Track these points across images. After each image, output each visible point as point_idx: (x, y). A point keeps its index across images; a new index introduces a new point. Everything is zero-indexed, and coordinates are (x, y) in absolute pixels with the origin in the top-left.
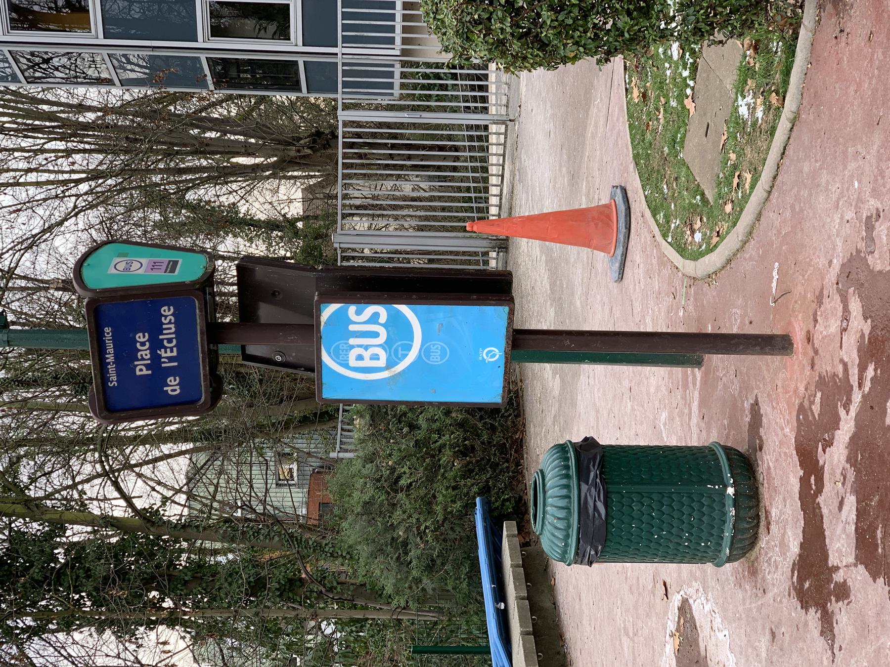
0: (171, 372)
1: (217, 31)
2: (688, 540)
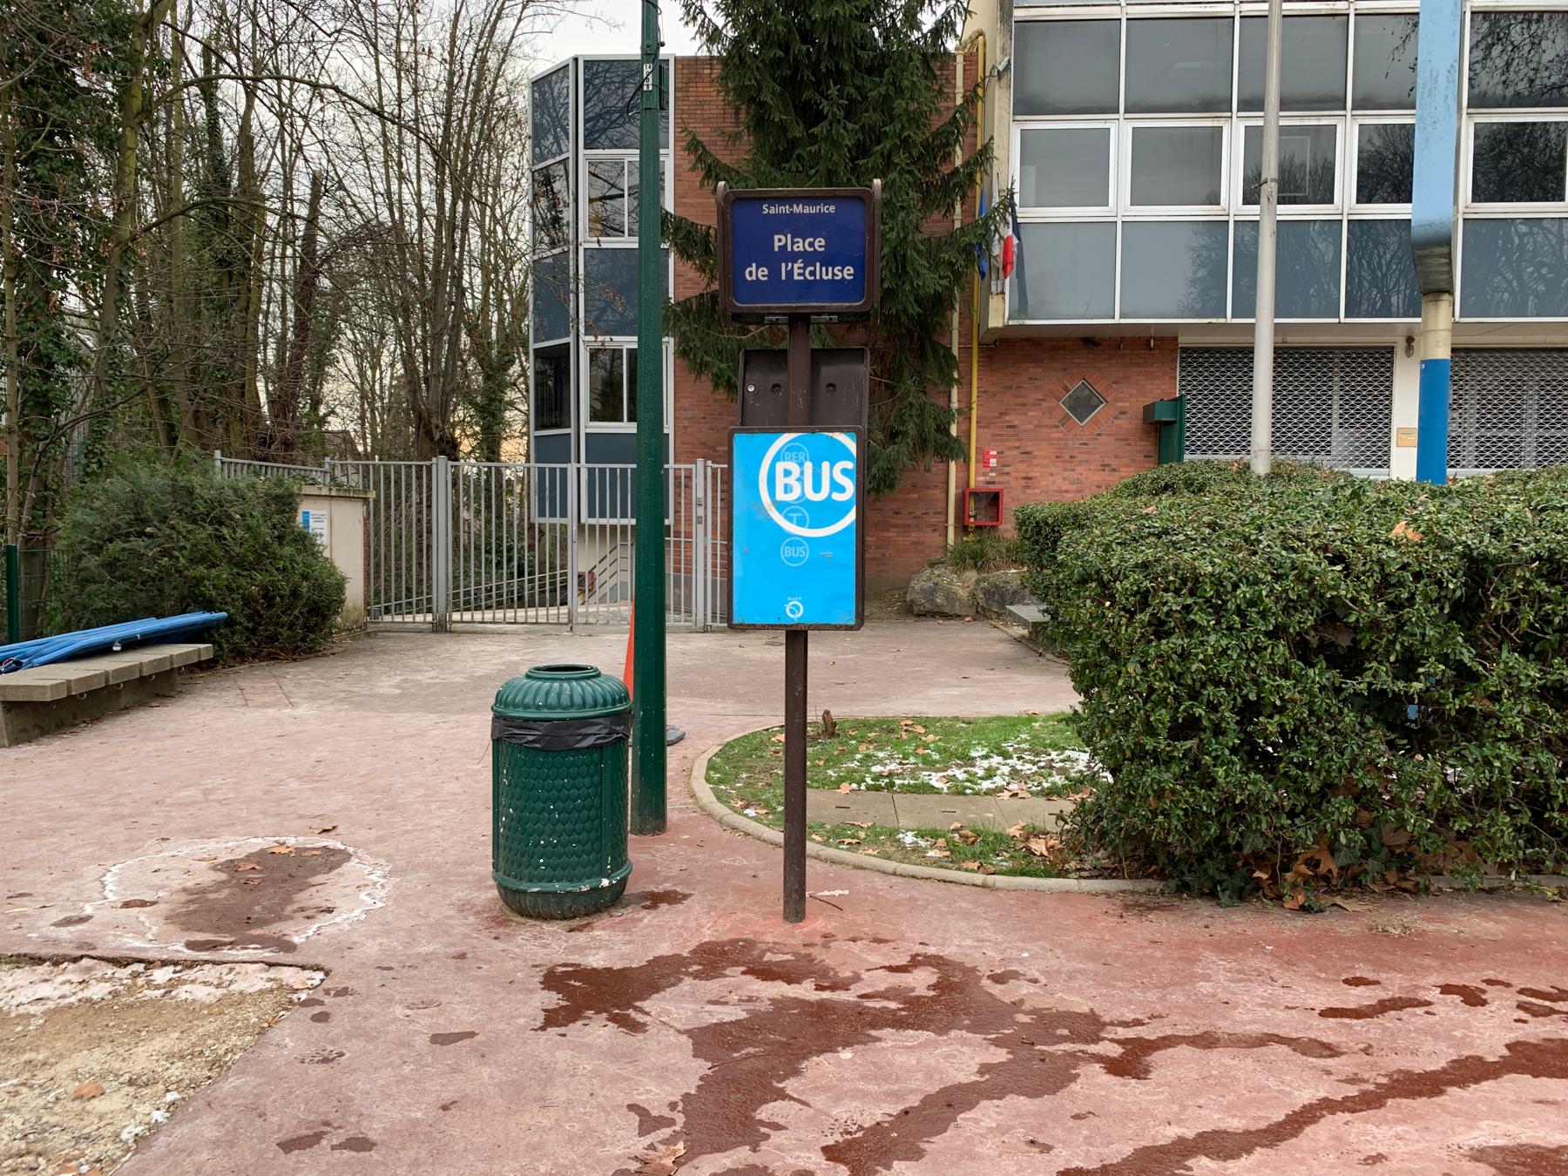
0: (774, 273)
1: (594, 354)
2: (548, 843)
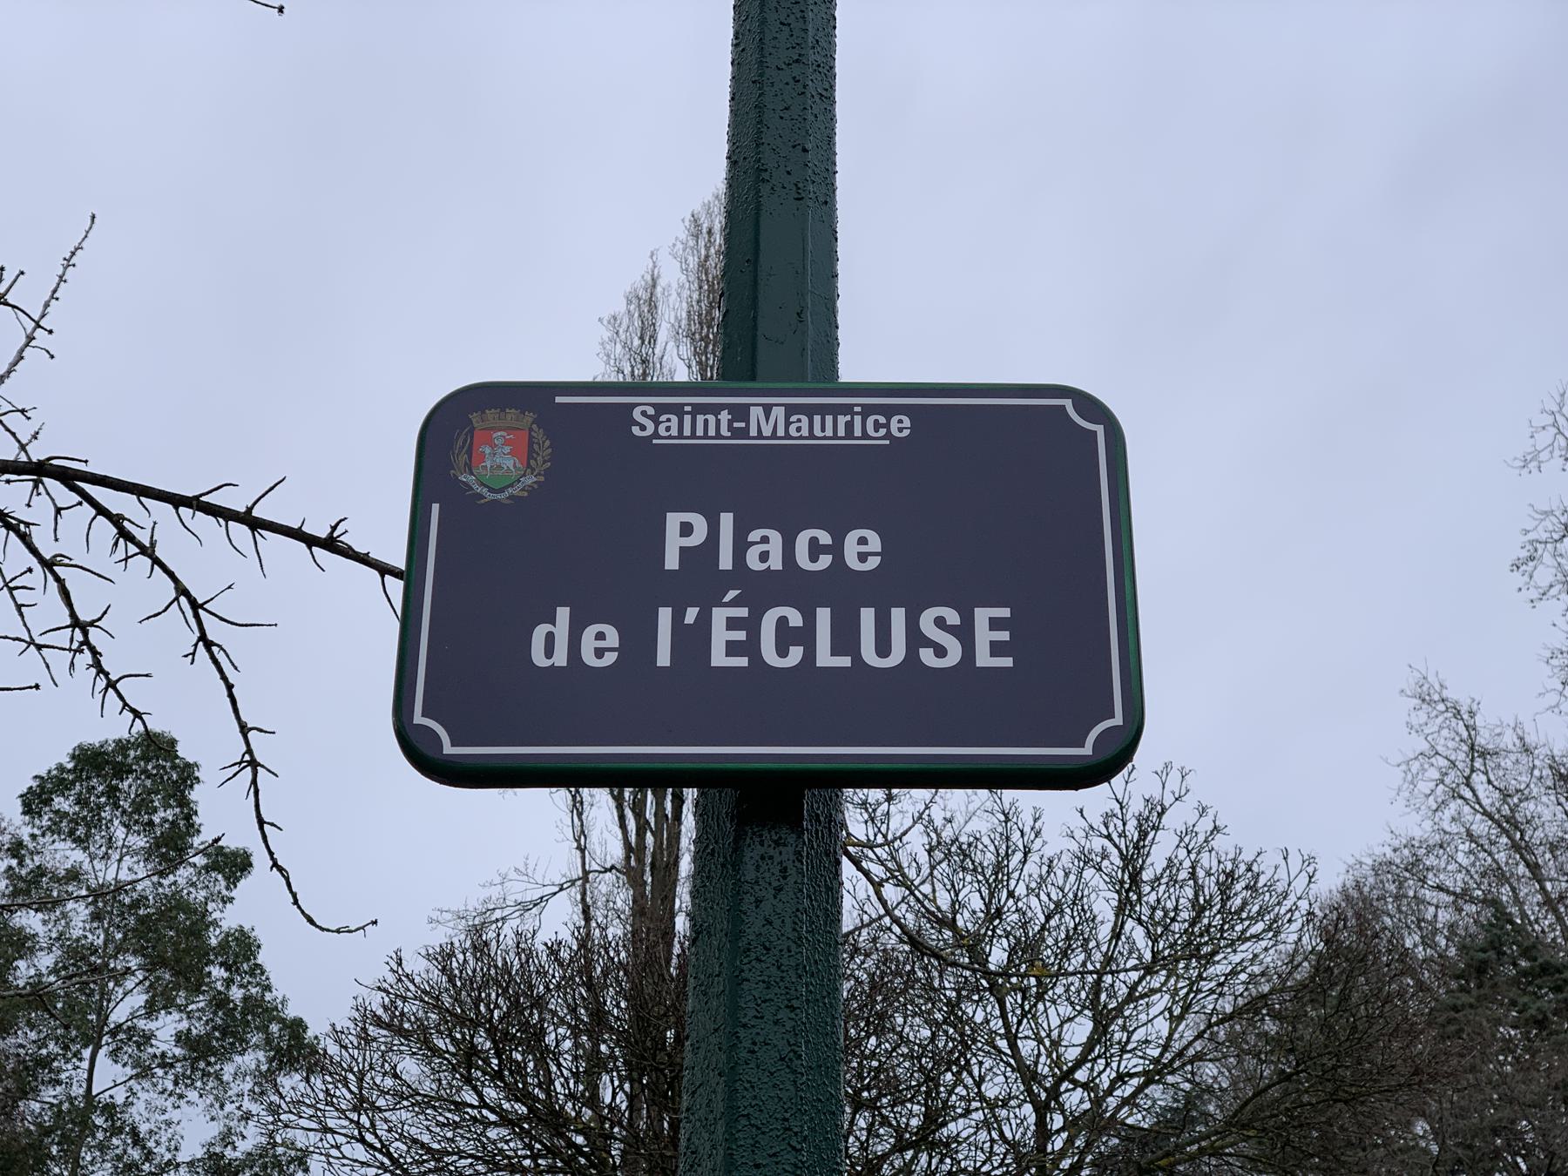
0: (638, 640)
